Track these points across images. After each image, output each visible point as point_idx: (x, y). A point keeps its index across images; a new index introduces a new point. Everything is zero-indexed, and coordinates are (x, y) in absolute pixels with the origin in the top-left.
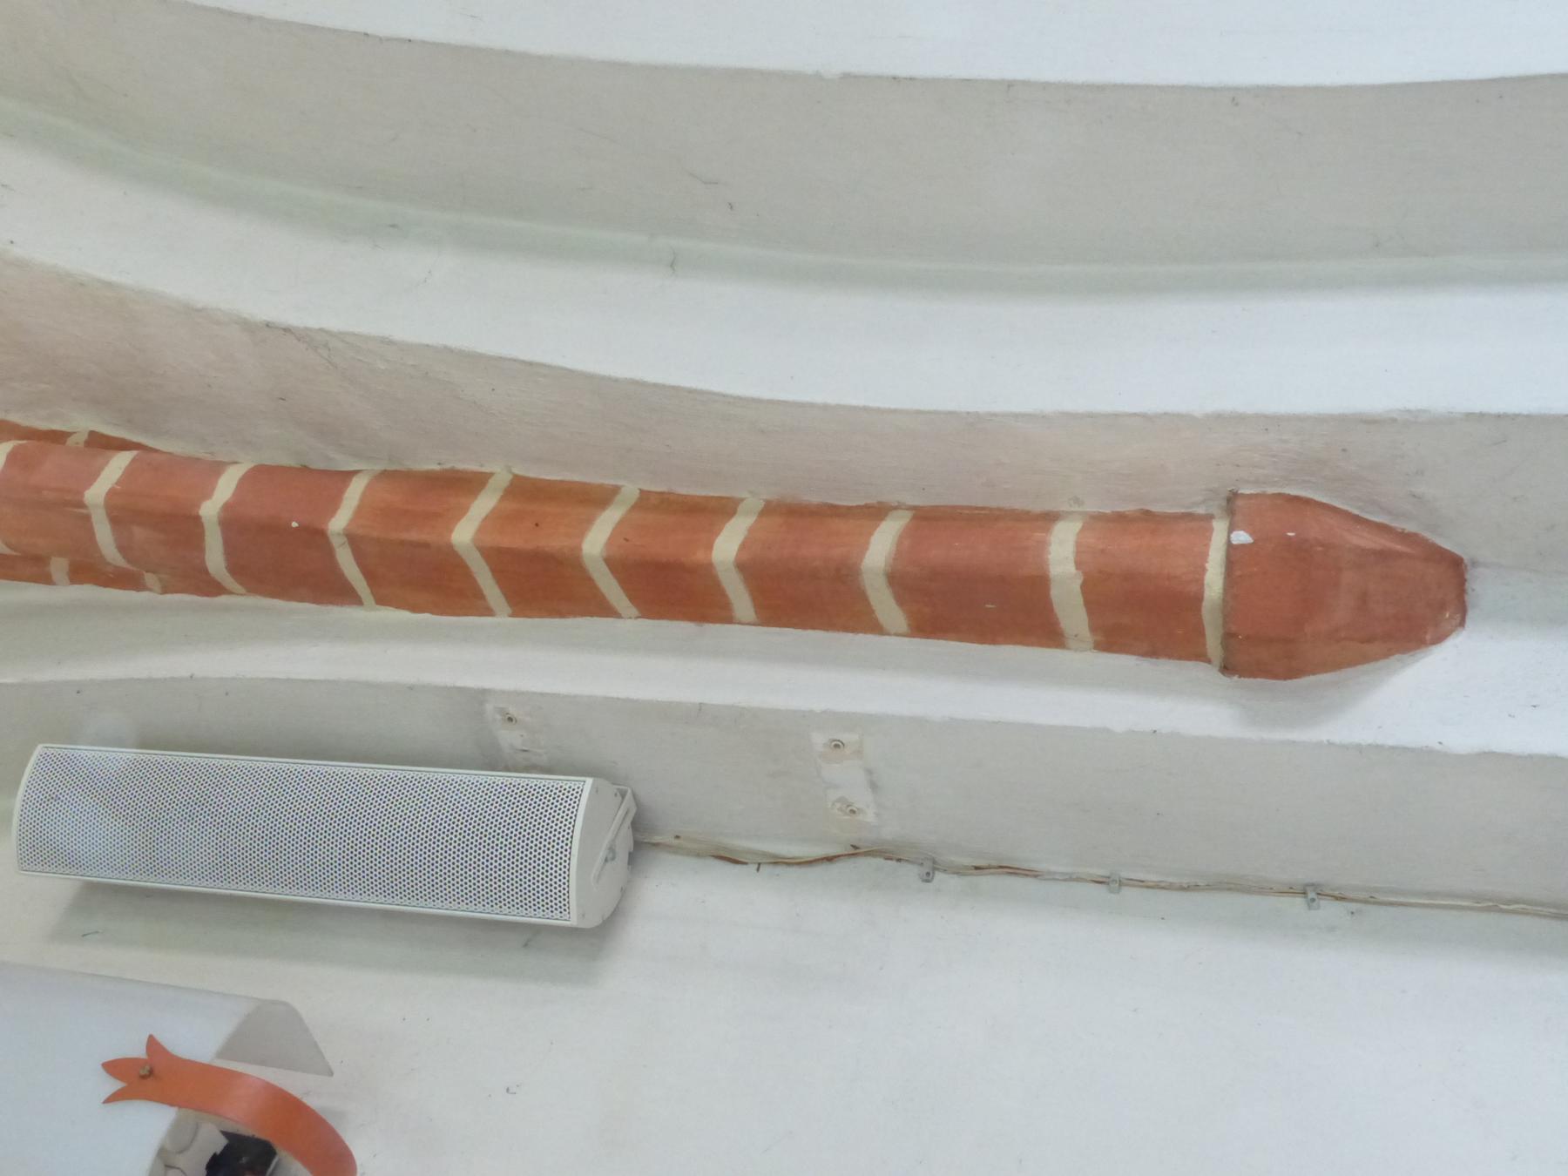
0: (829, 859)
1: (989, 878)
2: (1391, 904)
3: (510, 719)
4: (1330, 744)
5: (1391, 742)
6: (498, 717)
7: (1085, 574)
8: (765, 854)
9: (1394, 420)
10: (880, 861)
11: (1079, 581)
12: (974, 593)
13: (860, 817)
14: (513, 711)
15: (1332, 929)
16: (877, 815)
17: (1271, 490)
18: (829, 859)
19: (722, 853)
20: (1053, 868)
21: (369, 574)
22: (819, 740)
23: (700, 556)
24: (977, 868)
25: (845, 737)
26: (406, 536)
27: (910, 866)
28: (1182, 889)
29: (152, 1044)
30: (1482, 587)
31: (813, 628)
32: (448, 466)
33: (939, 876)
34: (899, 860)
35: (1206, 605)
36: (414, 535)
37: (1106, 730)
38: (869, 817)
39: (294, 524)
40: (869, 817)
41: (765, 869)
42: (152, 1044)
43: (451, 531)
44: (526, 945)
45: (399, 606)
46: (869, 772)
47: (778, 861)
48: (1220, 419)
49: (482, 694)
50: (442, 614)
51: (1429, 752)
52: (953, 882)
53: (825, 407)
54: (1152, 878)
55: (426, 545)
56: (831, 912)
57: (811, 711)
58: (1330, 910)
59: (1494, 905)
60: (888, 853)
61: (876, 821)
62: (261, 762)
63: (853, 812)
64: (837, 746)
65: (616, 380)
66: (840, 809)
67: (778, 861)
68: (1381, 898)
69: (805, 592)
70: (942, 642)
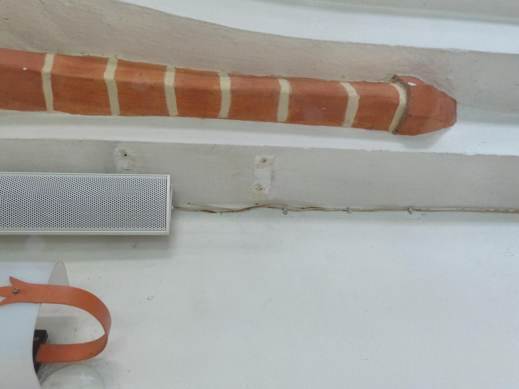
0: (249, 209)
1: (306, 212)
2: (433, 211)
3: (125, 155)
4: (434, 153)
5: (451, 152)
6: (120, 154)
7: (361, 96)
8: (224, 209)
9: (449, 52)
10: (266, 209)
11: (359, 98)
12: (318, 106)
13: (263, 191)
14: (128, 151)
15: (419, 219)
16: (270, 190)
17: (406, 75)
18: (249, 209)
19: (206, 208)
20: (329, 207)
21: (56, 95)
22: (258, 158)
23: (215, 87)
24: (302, 208)
25: (268, 157)
26: (80, 76)
27: (279, 210)
28: (371, 211)
29: (12, 279)
30: (460, 111)
31: (249, 120)
32: (86, 54)
33: (289, 212)
34: (273, 208)
35: (399, 107)
36: (85, 76)
37: (364, 151)
38: (266, 191)
39: (25, 69)
40: (266, 191)
41: (223, 214)
42: (12, 279)
43: (103, 75)
44: (134, 247)
45: (64, 111)
46: (273, 172)
47: (233, 211)
48: (399, 48)
49: (116, 143)
50: (87, 114)
51: (461, 155)
52: (295, 214)
53: (264, 35)
54: (361, 208)
55: (92, 80)
56: (256, 226)
57: (259, 146)
58: (416, 214)
59: (462, 209)
60: (270, 206)
61: (270, 193)
62: (12, 174)
63: (261, 189)
64: (264, 161)
65: (180, 17)
66: (256, 189)
67: (233, 211)
68: (431, 209)
69: (253, 104)
70: (297, 125)
